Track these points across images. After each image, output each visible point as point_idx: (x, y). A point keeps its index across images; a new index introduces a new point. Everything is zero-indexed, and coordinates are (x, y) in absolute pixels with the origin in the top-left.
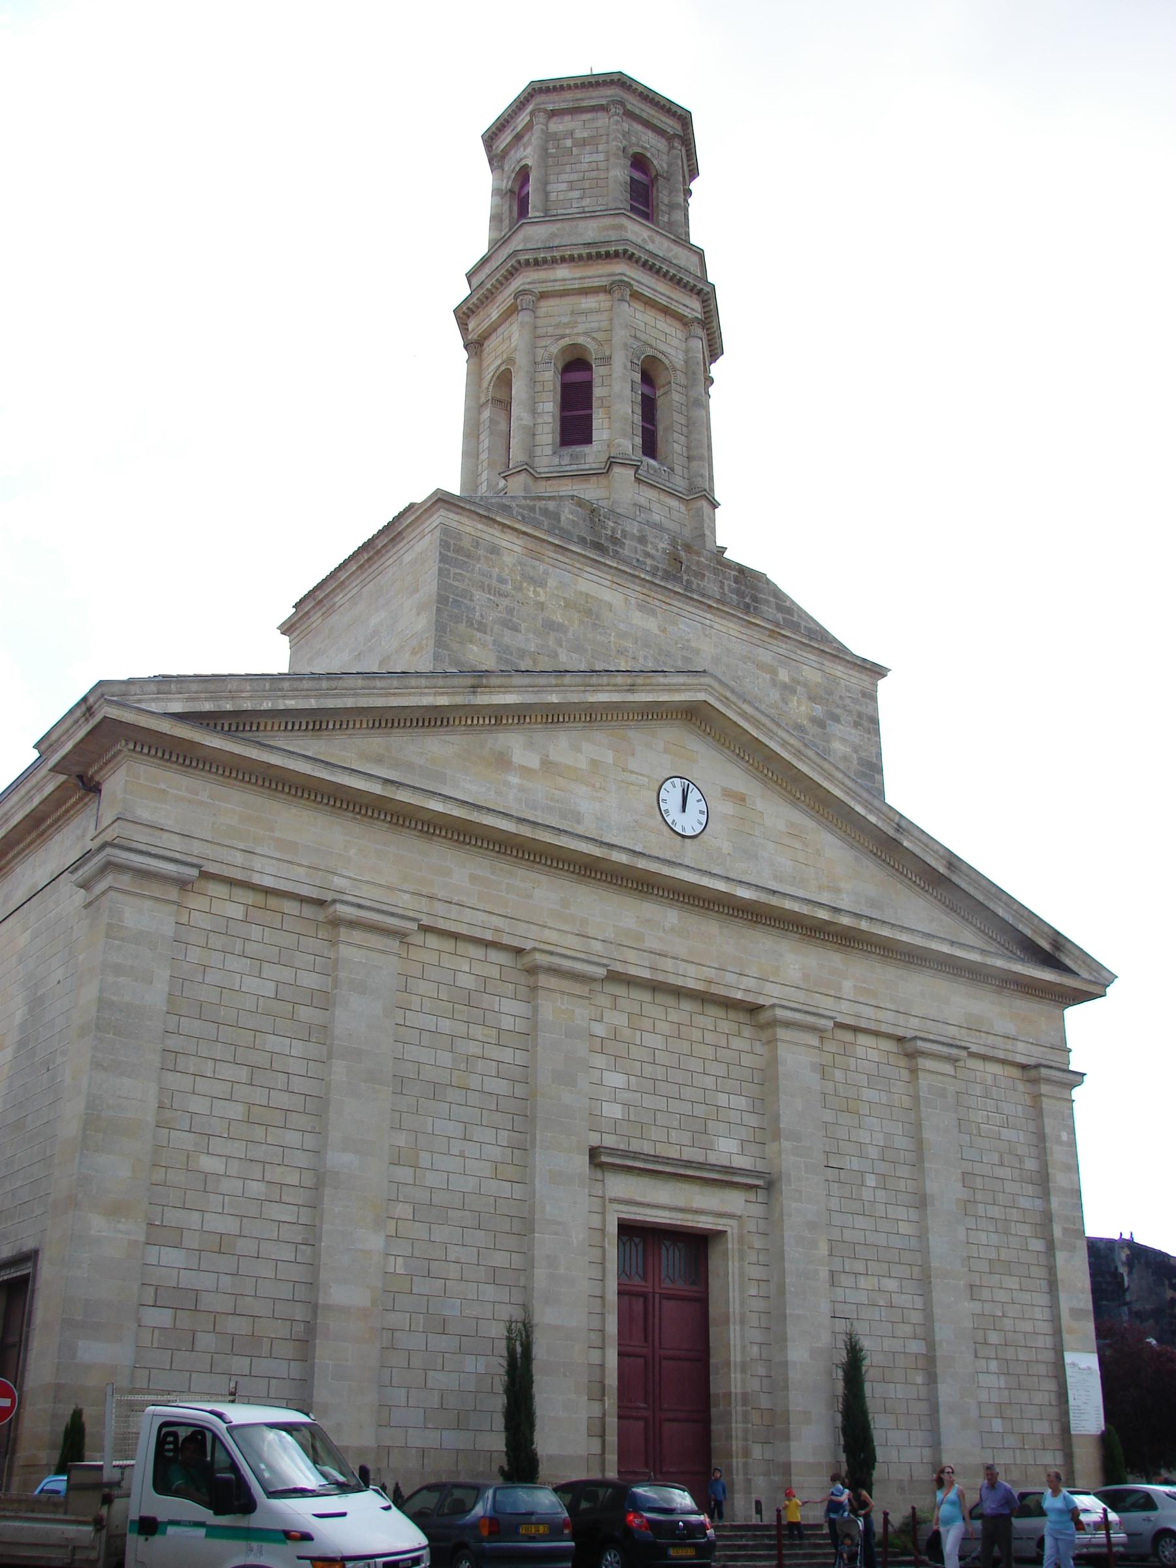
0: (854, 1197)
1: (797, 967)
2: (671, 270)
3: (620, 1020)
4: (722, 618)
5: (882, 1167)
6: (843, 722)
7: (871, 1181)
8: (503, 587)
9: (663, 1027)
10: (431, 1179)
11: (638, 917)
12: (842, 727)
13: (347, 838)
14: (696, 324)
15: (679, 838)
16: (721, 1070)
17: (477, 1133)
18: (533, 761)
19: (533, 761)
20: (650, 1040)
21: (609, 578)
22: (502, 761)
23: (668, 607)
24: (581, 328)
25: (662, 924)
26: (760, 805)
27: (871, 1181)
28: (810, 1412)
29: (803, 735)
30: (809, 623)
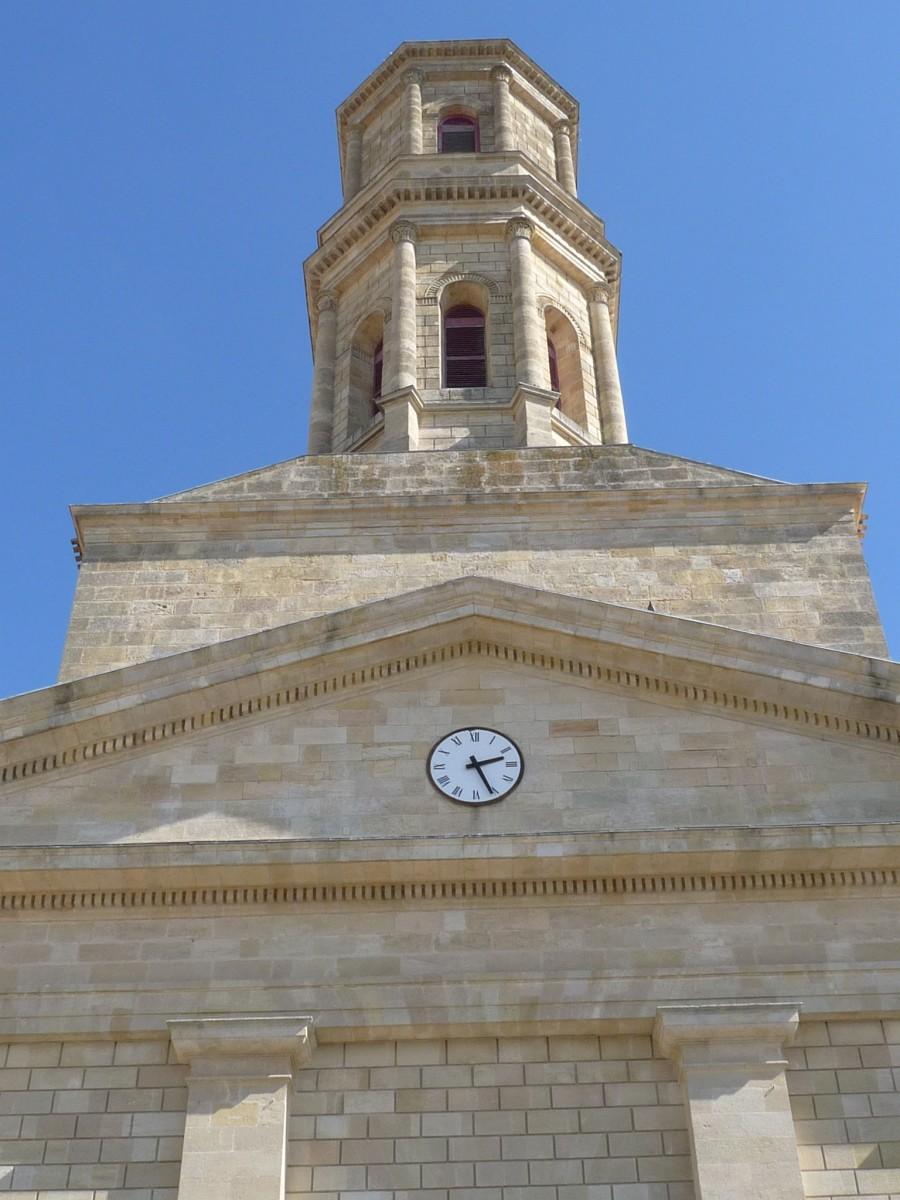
1: (721, 942)
2: (442, 186)
3: (379, 1103)
6: (786, 577)
8: (176, 585)
11: (386, 938)
12: (786, 584)
14: (515, 226)
15: (469, 809)
20: (436, 1124)
23: (449, 529)
24: (375, 296)
25: (434, 938)
26: (625, 726)
29: (709, 614)
30: (717, 477)
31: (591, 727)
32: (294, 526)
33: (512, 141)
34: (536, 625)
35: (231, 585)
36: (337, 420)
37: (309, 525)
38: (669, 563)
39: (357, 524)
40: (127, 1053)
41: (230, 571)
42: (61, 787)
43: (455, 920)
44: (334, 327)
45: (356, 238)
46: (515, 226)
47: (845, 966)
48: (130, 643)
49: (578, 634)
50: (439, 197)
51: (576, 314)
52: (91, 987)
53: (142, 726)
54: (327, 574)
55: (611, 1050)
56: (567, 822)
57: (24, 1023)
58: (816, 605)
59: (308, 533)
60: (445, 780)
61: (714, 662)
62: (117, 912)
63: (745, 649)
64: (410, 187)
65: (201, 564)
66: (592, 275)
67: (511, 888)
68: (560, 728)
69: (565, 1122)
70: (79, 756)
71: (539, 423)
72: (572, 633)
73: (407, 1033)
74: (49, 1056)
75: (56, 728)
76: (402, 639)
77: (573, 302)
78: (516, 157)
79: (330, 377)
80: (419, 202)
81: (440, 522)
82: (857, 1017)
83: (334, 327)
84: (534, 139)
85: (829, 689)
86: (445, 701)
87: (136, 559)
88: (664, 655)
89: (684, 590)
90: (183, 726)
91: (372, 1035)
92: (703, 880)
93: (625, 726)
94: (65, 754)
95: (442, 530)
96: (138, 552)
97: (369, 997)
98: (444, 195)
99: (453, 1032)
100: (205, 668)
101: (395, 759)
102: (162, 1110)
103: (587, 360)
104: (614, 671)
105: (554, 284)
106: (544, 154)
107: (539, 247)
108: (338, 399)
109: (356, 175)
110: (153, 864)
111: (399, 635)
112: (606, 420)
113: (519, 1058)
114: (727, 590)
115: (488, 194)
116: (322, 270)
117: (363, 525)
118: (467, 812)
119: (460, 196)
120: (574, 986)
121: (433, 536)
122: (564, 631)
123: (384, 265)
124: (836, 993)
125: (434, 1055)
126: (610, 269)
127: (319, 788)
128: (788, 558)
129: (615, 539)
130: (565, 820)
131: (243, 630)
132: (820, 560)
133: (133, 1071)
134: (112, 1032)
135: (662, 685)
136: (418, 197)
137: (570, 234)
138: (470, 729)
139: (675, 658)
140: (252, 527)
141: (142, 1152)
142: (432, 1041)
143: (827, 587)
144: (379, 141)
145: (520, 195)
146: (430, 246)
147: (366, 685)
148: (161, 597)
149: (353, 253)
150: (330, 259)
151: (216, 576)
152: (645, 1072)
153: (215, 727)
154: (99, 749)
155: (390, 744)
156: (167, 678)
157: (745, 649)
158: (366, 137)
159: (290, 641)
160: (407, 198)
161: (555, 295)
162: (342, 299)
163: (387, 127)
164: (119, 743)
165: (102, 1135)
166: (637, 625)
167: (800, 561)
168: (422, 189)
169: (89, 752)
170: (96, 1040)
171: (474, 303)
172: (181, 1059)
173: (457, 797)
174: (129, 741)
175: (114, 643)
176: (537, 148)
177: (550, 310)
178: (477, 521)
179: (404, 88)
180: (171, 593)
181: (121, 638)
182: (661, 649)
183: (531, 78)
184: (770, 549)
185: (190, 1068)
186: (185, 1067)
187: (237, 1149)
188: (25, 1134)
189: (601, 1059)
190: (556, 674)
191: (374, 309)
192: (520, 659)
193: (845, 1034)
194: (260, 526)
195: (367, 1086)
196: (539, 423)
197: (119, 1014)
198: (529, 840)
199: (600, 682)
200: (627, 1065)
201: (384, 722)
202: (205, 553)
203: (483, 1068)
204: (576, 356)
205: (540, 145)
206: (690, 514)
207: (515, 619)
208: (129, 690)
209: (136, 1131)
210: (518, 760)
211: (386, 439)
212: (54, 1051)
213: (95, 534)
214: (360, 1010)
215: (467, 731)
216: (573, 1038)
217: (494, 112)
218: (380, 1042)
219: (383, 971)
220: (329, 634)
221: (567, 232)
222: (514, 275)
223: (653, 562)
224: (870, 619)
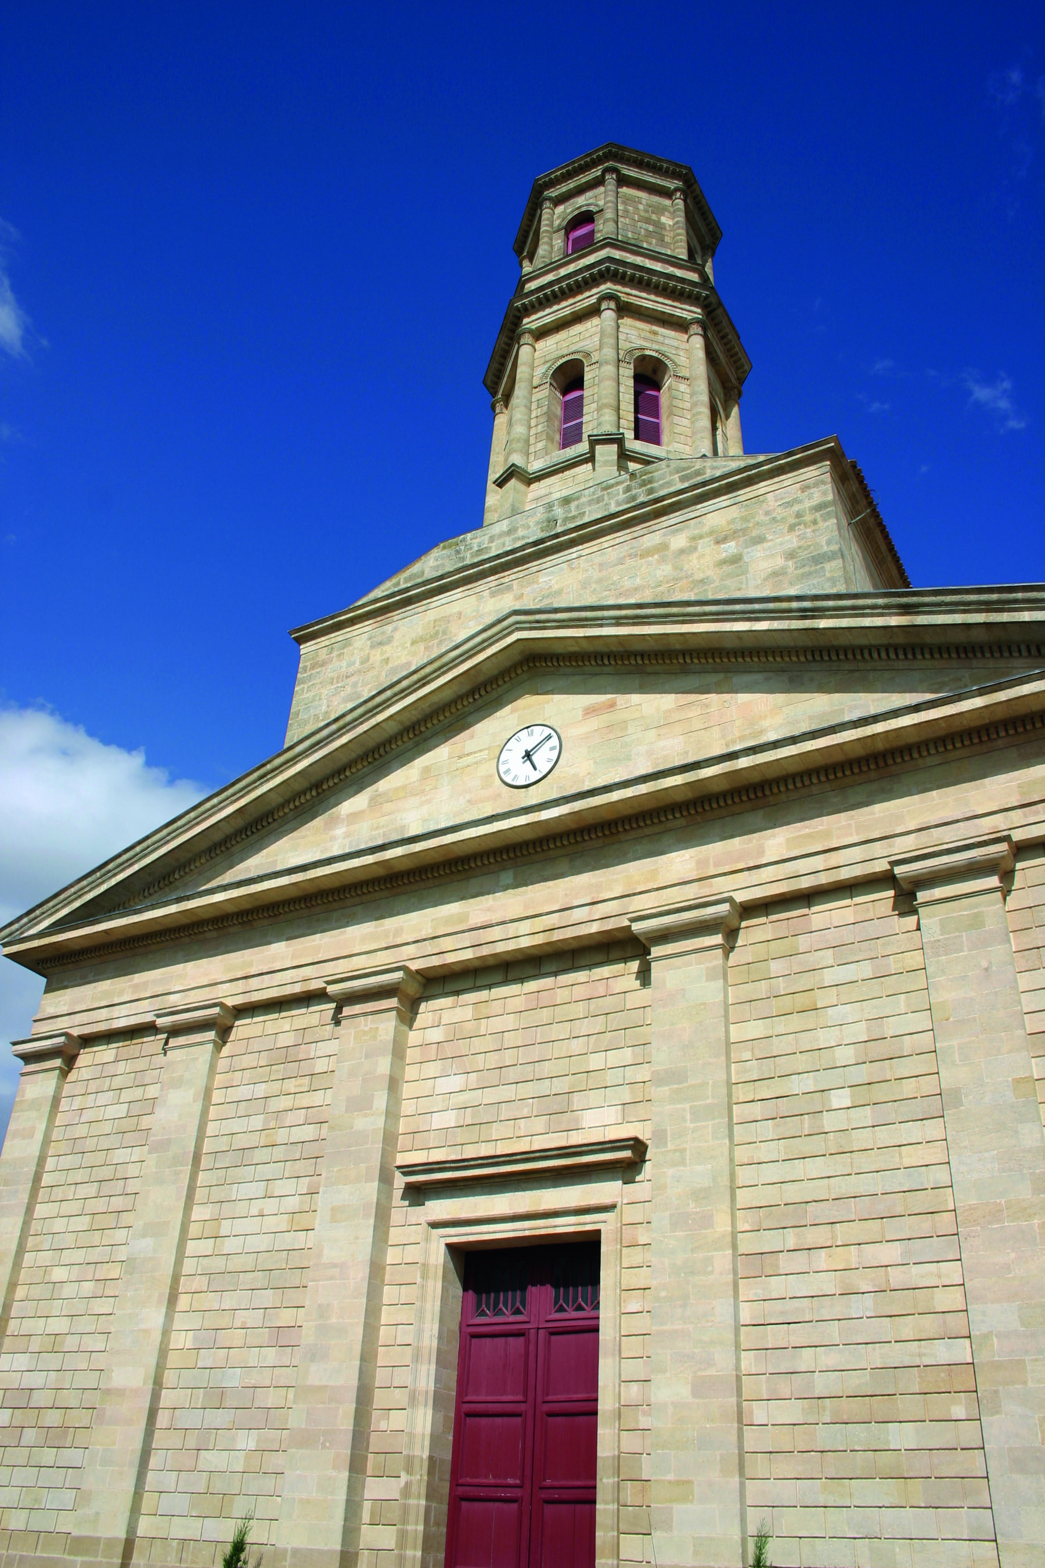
5: (863, 1074)
7: (841, 1099)
10: (230, 1245)
92: (1000, 647)
105: (648, 334)
132: (798, 515)
137: (660, 288)
145: (606, 275)
180: (349, 677)
183: (640, 165)
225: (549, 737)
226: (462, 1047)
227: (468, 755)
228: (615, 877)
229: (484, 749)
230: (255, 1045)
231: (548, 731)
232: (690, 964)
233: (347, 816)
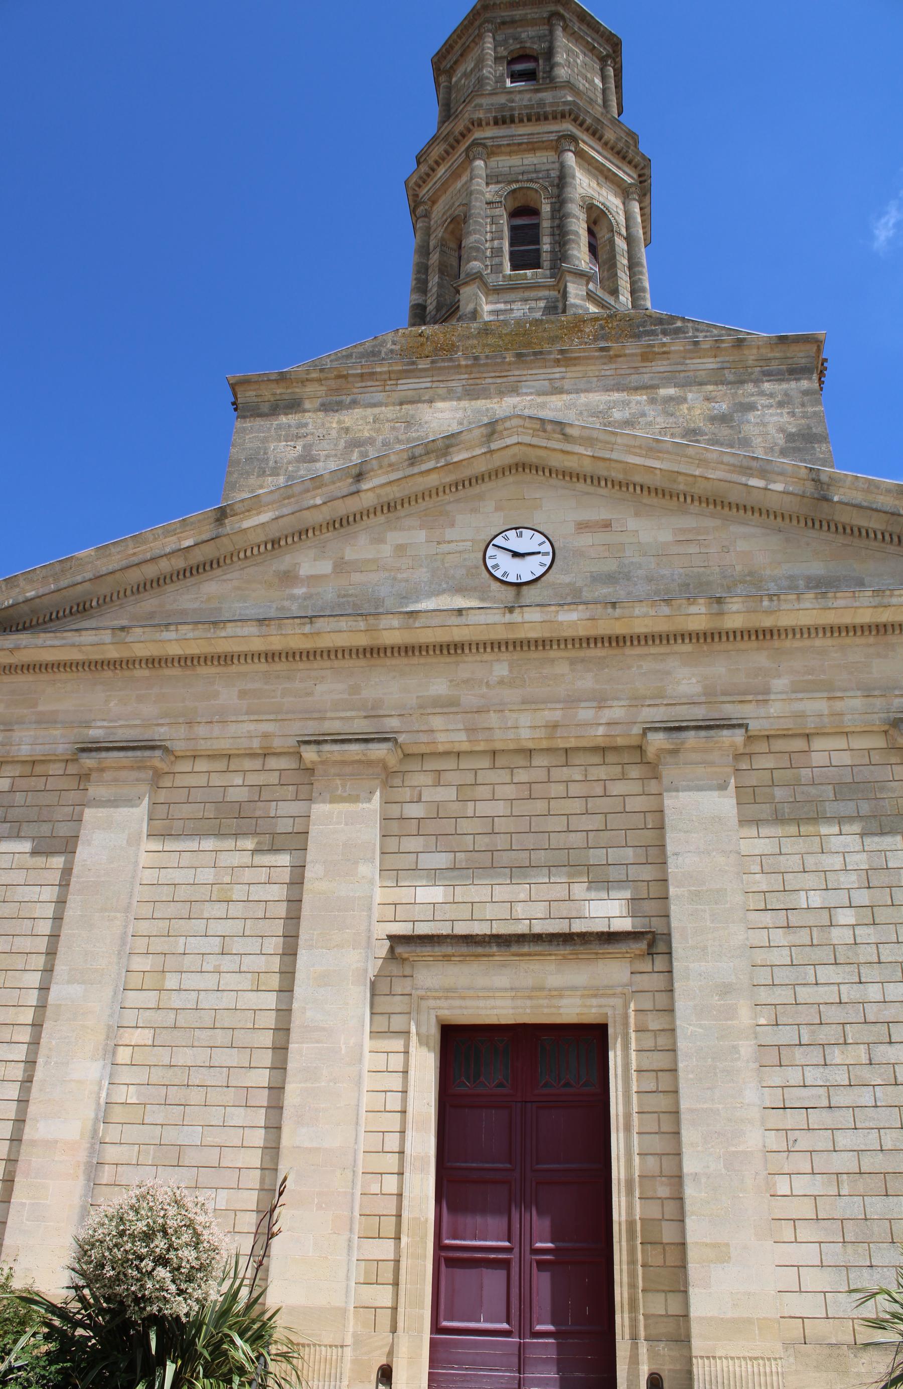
0: (815, 942)
1: (694, 680)
4: (575, 365)
8: (303, 431)
9: (509, 791)
11: (451, 681)
13: (108, 693)
16: (596, 822)
17: (238, 946)
18: (325, 567)
19: (325, 567)
20: (484, 808)
21: (429, 379)
22: (288, 577)
23: (504, 380)
27: (846, 917)
28: (727, 1245)
31: (607, 525)
32: (389, 382)
33: (562, 73)
34: (564, 449)
35: (342, 428)
36: (429, 301)
37: (400, 382)
38: (671, 399)
39: (435, 379)
40: (272, 763)
41: (342, 418)
42: (225, 581)
43: (501, 669)
44: (428, 232)
45: (443, 159)
46: (563, 141)
47: (784, 696)
48: (270, 475)
49: (596, 455)
50: (504, 123)
51: (613, 209)
52: (245, 718)
53: (277, 535)
54: (413, 417)
55: (611, 758)
56: (586, 595)
57: (202, 742)
58: (782, 430)
59: (400, 387)
60: (496, 566)
61: (697, 473)
62: (263, 667)
63: (722, 463)
64: (481, 116)
65: (321, 415)
66: (626, 178)
67: (543, 644)
68: (583, 527)
69: (577, 806)
70: (235, 559)
71: (577, 296)
72: (591, 454)
73: (465, 747)
74: (221, 765)
75: (217, 537)
76: (464, 463)
77: (612, 201)
78: (569, 85)
79: (423, 269)
80: (489, 127)
81: (497, 374)
82: (790, 732)
83: (428, 232)
84: (584, 71)
85: (784, 492)
86: (497, 509)
87: (274, 415)
88: (660, 469)
89: (681, 420)
90: (307, 534)
91: (441, 749)
92: (683, 635)
93: (632, 524)
94: (225, 557)
95: (499, 380)
96: (276, 409)
97: (437, 722)
98: (508, 121)
99: (498, 746)
100: (320, 491)
101: (460, 552)
102: (296, 799)
103: (621, 244)
104: (624, 482)
106: (592, 82)
107: (580, 155)
108: (430, 285)
109: (448, 112)
110: (284, 632)
111: (462, 461)
112: (635, 291)
113: (545, 763)
114: (713, 419)
115: (542, 118)
116: (420, 186)
117: (440, 379)
118: (512, 591)
119: (521, 121)
120: (585, 714)
121: (492, 386)
122: (585, 453)
123: (464, 179)
124: (775, 715)
125: (486, 763)
126: (642, 172)
127: (405, 575)
128: (762, 393)
129: (630, 382)
130: (584, 593)
131: (351, 461)
133: (277, 773)
134: (261, 748)
135: (660, 492)
136: (488, 124)
138: (516, 529)
139: (668, 471)
140: (359, 385)
141: (285, 826)
142: (484, 752)
143: (792, 414)
144: (463, 81)
146: (498, 161)
147: (439, 499)
148: (292, 440)
149: (441, 171)
150: (425, 177)
151: (332, 423)
152: (634, 772)
153: (330, 534)
154: (249, 553)
155: (456, 541)
156: (292, 500)
157: (722, 463)
158: (454, 80)
159: (381, 467)
160: (480, 125)
161: (596, 195)
162: (435, 207)
163: (469, 69)
164: (262, 548)
165: (257, 815)
166: (640, 447)
167: (771, 395)
168: (491, 116)
169: (242, 555)
170: (253, 755)
171: (532, 204)
172: (309, 766)
173: (504, 579)
174: (269, 546)
175: (258, 476)
176: (586, 79)
177: (591, 208)
178: (525, 372)
179: (480, 36)
181: (264, 472)
182: (657, 464)
184: (750, 387)
185: (313, 775)
186: (311, 771)
187: (346, 824)
188: (207, 815)
189: (604, 764)
190: (581, 486)
191: (457, 213)
192: (554, 475)
193: (779, 745)
194: (364, 384)
195: (437, 784)
196: (577, 296)
197: (266, 736)
198: (553, 608)
199: (613, 491)
200: (623, 768)
201: (453, 525)
202: (326, 408)
203: (520, 770)
204: (612, 242)
205: (589, 75)
206: (688, 361)
207: (548, 445)
208: (266, 508)
209: (279, 813)
210: (551, 551)
211: (460, 313)
212: (225, 762)
213: (247, 395)
214: (432, 731)
215: (514, 531)
216: (585, 749)
217: (550, 53)
218: (447, 753)
219: (446, 705)
220: (410, 461)
221: (606, 144)
222: (562, 181)
223: (659, 399)
224: (822, 439)
225: (547, 554)
226: (448, 826)
227: (449, 542)
228: (620, 687)
229: (467, 540)
230: (197, 795)
231: (547, 547)
232: (237, 626)
233: (307, 577)
